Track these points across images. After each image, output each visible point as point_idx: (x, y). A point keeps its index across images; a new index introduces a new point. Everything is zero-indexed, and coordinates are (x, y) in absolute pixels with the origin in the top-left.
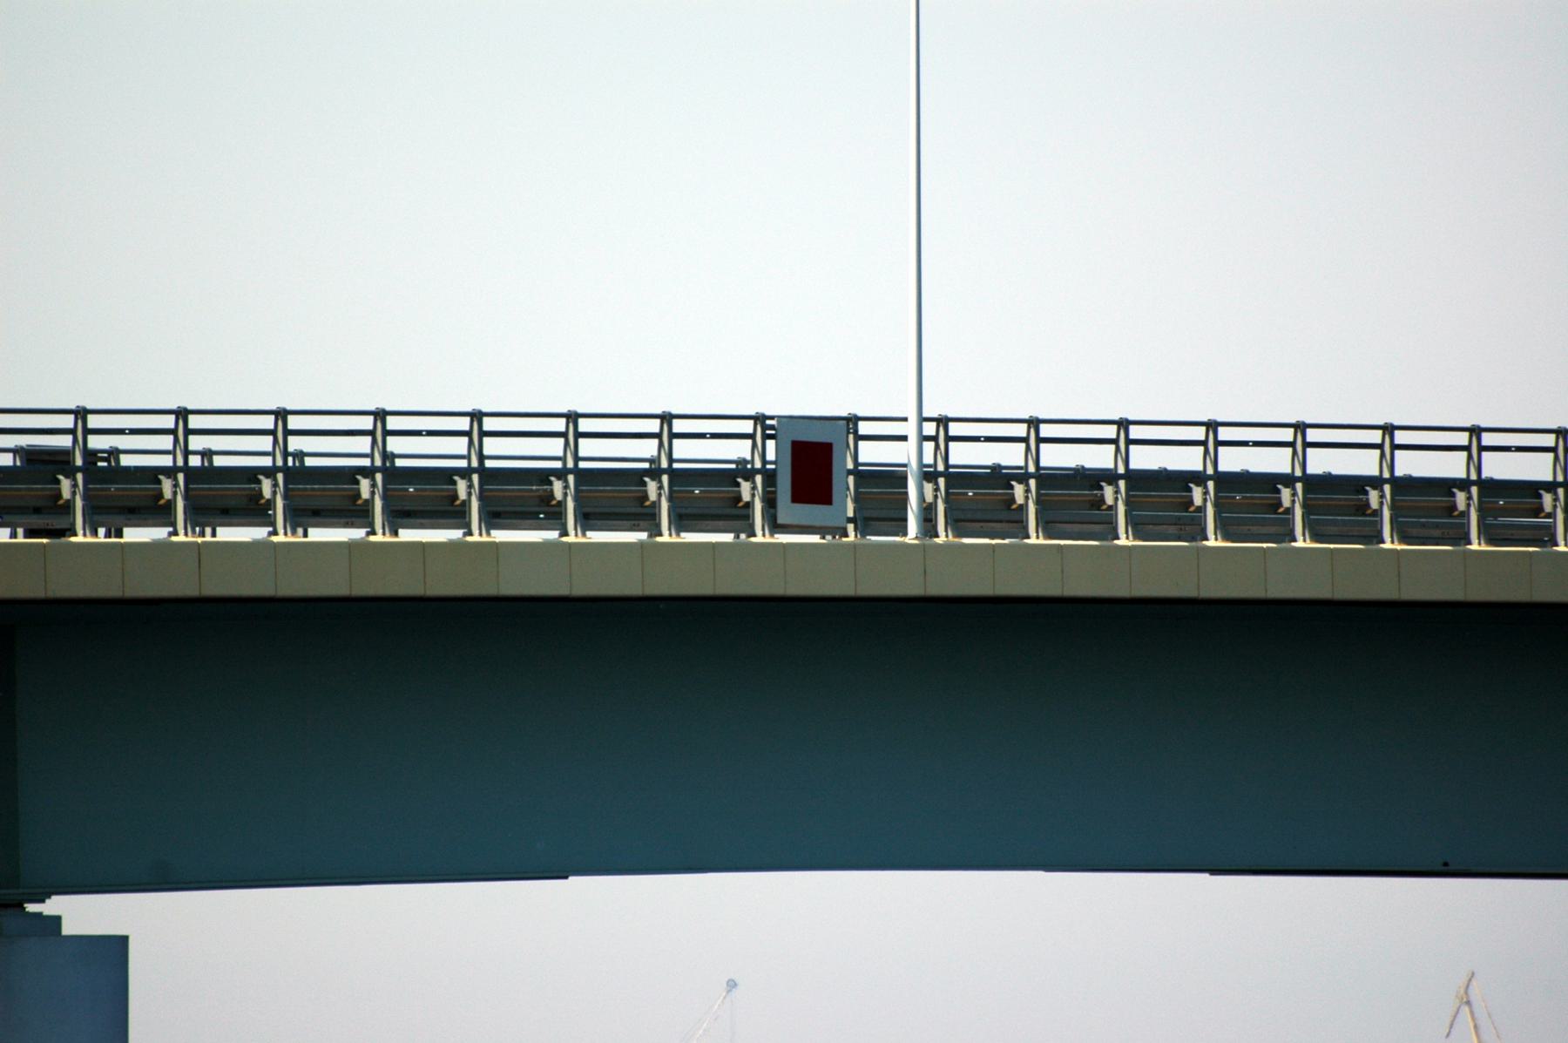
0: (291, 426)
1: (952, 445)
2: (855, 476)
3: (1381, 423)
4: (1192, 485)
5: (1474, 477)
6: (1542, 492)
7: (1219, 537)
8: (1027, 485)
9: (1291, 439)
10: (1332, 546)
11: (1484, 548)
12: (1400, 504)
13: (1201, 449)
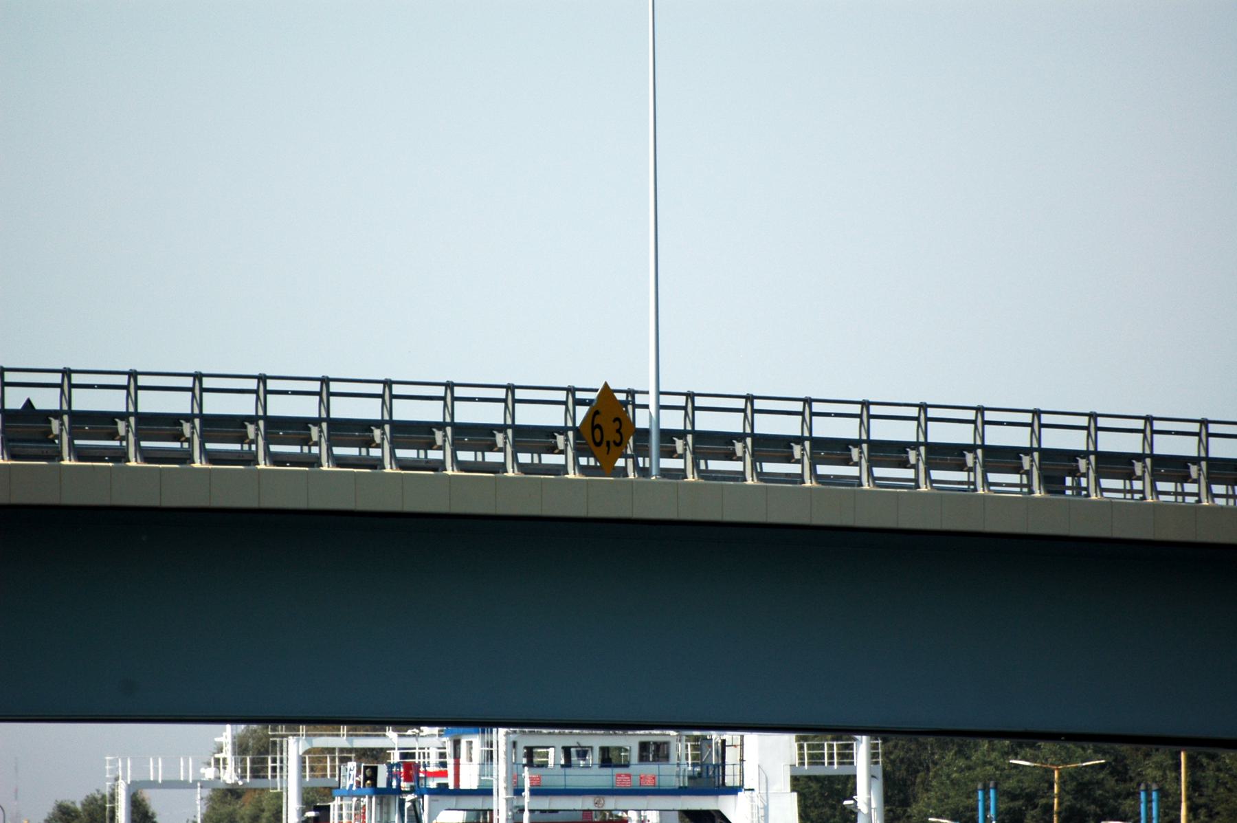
0: (697, 404)
1: (697, 413)
2: (69, 416)
3: (861, 400)
4: (965, 452)
5: (806, 434)
6: (310, 425)
7: (455, 469)
8: (321, 427)
9: (255, 388)
10: (161, 466)
11: (73, 463)
12: (699, 451)
13: (125, 392)
